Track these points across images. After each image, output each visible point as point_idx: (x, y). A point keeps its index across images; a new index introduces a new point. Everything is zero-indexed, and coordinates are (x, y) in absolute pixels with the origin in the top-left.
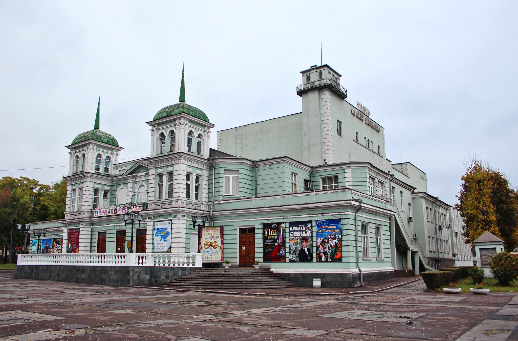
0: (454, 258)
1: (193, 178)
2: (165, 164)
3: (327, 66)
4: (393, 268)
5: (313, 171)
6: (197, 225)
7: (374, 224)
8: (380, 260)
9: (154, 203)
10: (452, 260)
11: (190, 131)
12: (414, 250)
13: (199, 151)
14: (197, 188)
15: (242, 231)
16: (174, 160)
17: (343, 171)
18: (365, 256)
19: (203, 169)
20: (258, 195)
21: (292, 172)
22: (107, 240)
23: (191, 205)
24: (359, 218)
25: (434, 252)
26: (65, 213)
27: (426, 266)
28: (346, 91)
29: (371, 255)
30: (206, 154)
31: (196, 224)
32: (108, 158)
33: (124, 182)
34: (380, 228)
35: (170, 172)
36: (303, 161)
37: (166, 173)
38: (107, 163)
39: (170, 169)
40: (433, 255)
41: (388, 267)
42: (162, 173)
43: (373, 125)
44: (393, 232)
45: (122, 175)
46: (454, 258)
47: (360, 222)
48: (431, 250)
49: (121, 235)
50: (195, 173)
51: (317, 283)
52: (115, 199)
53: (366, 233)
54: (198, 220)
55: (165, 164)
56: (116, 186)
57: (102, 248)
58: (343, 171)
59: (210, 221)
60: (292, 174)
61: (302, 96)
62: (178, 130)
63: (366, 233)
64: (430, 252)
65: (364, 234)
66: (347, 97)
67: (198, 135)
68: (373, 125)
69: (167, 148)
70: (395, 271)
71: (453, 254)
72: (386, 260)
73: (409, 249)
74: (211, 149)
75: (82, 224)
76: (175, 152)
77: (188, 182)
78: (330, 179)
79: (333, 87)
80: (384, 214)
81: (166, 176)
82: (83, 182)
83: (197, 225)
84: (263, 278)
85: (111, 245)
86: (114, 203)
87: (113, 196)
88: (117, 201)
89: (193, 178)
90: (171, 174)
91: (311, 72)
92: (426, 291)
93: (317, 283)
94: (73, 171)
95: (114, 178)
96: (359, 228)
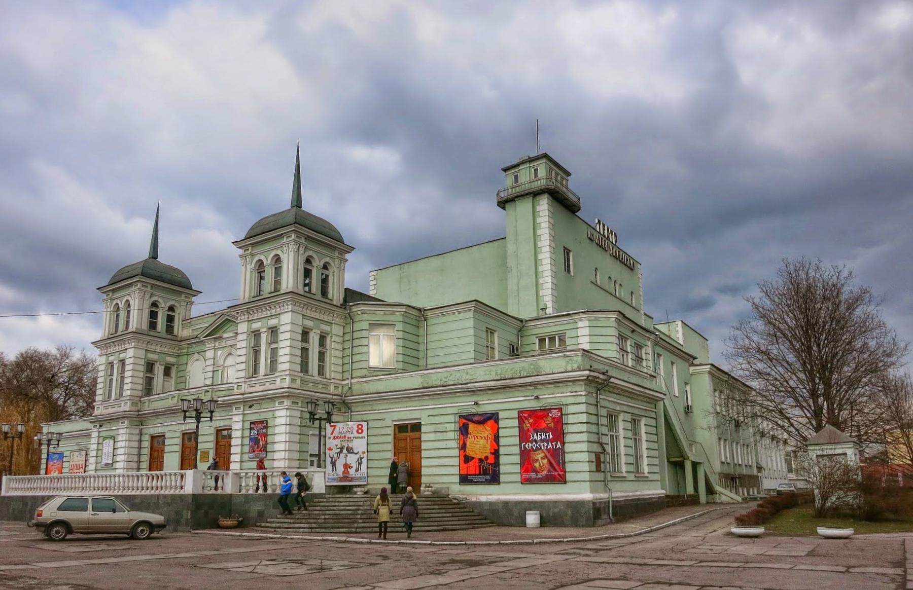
0: (759, 475)
1: (314, 339)
2: (265, 314)
3: (545, 156)
4: (664, 492)
5: (523, 327)
6: (317, 419)
7: (630, 415)
8: (640, 478)
9: (245, 382)
10: (757, 477)
11: (308, 256)
12: (697, 461)
13: (324, 292)
14: (322, 356)
15: (401, 428)
16: (280, 307)
17: (571, 326)
18: (615, 471)
19: (332, 323)
20: (429, 367)
21: (486, 328)
22: (167, 449)
23: (311, 384)
24: (602, 403)
25: (728, 463)
26: (94, 404)
27: (718, 488)
28: (579, 199)
29: (624, 468)
30: (336, 294)
31: (315, 417)
32: (171, 309)
33: (199, 348)
34: (639, 421)
35: (273, 328)
36: (506, 304)
37: (265, 330)
38: (170, 319)
39: (273, 322)
40: (726, 470)
41: (654, 490)
42: (259, 331)
43: (622, 259)
44: (662, 429)
45: (197, 337)
46: (759, 475)
47: (606, 410)
48: (723, 460)
49: (190, 440)
50: (318, 328)
51: (532, 518)
52: (184, 378)
53: (616, 430)
54: (318, 411)
55: (265, 314)
56: (186, 356)
57: (156, 462)
58: (571, 326)
59: (345, 413)
60: (487, 331)
61: (506, 208)
62: (286, 255)
63: (616, 430)
64: (722, 463)
65: (613, 432)
66: (579, 209)
67: (324, 265)
68: (622, 259)
69: (268, 286)
70: (667, 497)
71: (757, 467)
72: (652, 477)
73: (688, 458)
74: (346, 289)
75: (122, 423)
76: (282, 292)
77: (305, 345)
78: (552, 339)
79: (558, 192)
80: (646, 397)
81: (266, 334)
82: (126, 349)
83: (317, 419)
84: (433, 511)
85: (172, 460)
86: (182, 386)
87: (180, 374)
88: (187, 382)
89: (314, 339)
90: (274, 331)
91: (521, 167)
92: (813, 517)
93: (532, 518)
94: (109, 331)
95: (183, 343)
96: (604, 421)
